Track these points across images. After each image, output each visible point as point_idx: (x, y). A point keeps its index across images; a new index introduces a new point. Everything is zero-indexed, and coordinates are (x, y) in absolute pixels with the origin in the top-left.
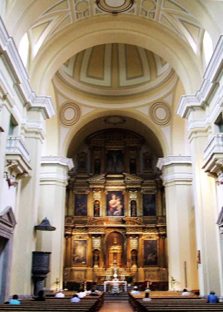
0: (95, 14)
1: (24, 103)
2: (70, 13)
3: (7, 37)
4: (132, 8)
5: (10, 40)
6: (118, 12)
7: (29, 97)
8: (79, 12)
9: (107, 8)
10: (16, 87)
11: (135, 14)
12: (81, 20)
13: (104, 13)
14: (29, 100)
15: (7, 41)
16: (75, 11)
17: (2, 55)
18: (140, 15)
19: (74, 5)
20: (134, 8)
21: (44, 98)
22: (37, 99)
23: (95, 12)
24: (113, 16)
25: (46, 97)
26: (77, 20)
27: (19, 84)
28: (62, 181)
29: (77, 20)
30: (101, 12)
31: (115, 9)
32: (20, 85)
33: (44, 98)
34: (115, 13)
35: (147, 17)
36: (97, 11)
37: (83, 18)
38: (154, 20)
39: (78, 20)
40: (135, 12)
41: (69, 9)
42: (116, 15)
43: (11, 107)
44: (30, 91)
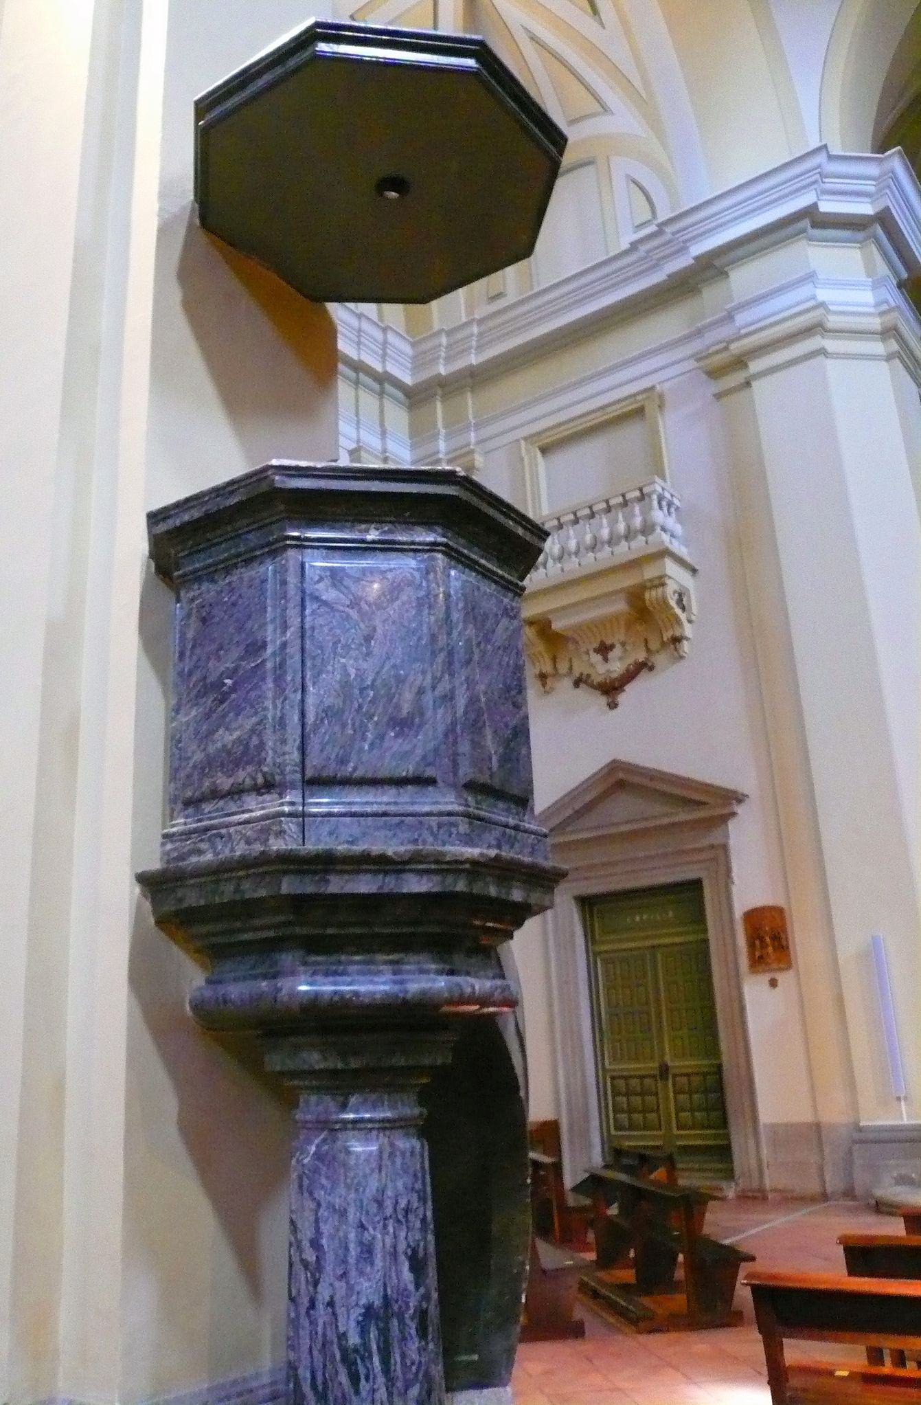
28: (876, 323)
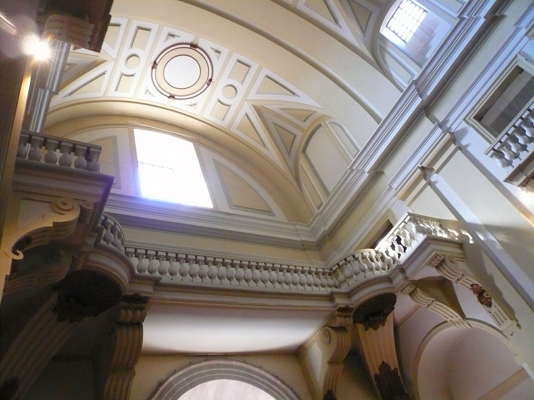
5: (465, 16)
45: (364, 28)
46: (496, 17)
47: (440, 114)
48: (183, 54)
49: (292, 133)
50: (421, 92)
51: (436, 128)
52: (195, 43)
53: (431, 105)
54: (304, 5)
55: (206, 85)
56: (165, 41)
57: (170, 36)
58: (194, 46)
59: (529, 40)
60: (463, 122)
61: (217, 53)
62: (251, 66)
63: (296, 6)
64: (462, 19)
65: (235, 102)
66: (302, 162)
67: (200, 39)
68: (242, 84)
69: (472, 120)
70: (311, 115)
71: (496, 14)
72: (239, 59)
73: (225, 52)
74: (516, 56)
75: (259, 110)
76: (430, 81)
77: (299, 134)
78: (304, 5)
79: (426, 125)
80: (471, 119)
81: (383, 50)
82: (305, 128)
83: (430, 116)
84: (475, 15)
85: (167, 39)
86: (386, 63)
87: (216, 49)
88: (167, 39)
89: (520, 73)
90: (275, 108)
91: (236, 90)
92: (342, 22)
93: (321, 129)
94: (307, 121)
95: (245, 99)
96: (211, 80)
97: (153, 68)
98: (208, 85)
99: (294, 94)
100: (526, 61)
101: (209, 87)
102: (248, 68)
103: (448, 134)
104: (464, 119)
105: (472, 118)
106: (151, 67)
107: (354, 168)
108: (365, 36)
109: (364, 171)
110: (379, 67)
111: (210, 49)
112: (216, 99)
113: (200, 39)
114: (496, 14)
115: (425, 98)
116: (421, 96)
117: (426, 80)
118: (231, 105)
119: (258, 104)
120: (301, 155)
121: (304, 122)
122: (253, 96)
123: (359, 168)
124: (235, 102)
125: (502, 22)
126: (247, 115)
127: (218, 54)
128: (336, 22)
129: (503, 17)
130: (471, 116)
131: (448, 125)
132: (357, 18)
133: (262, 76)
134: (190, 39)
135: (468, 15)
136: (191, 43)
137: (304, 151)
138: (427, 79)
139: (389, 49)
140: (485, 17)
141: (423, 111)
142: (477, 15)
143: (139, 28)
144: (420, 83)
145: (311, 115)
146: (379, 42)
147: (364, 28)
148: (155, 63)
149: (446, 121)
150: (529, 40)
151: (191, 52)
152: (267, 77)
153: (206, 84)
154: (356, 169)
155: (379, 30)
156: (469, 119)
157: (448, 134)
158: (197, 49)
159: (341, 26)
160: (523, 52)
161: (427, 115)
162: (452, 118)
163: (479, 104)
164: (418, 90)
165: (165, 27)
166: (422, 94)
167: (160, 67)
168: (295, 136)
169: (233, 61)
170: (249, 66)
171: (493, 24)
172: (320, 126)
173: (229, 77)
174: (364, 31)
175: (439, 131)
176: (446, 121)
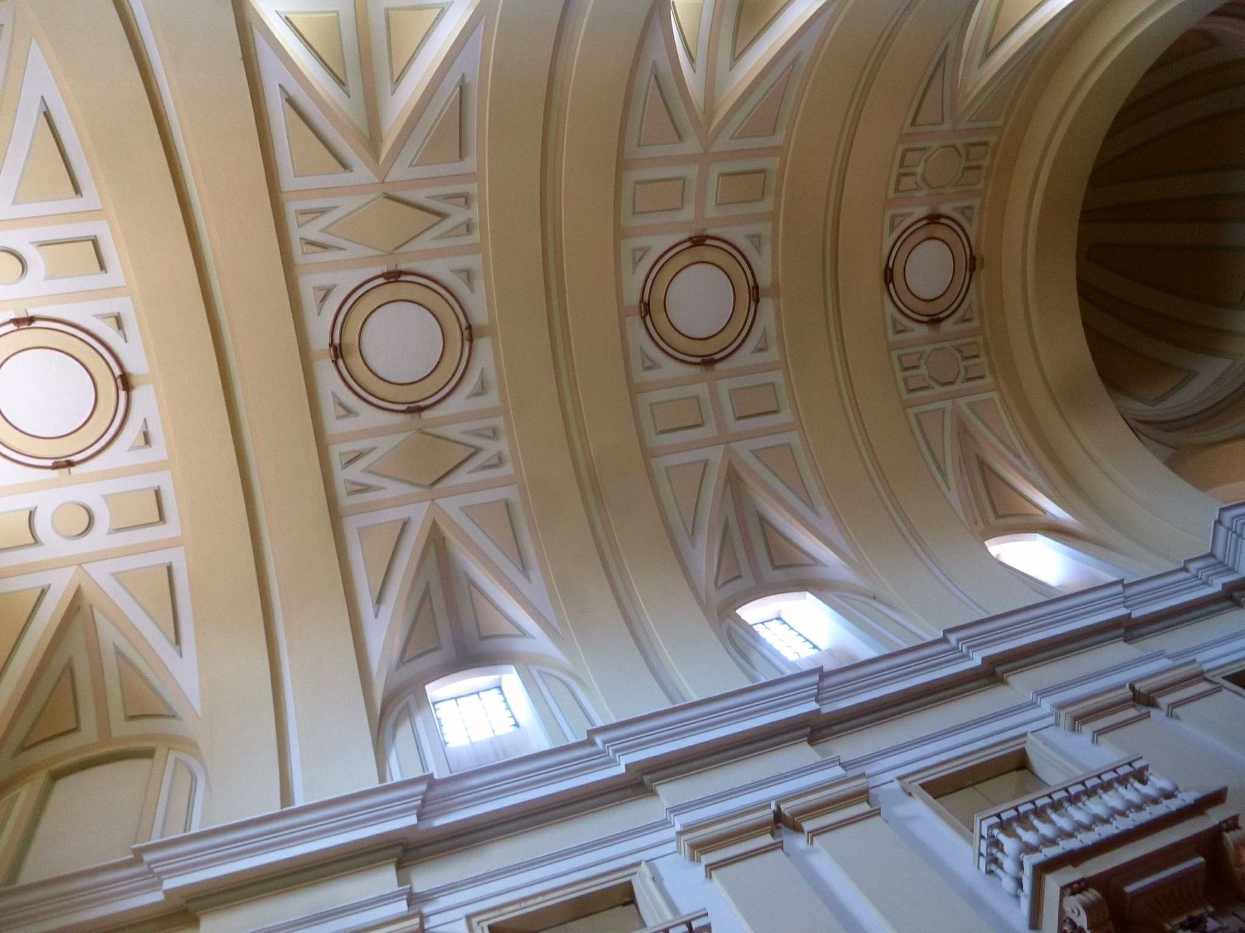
0: (976, 323)
1: (1229, 603)
2: (962, 402)
3: (944, 647)
4: (958, 217)
5: (598, 740)
6: (971, 251)
7: (1206, 583)
8: (963, 373)
9: (952, 295)
10: (1136, 633)
11: (977, 203)
12: (991, 366)
13: (972, 295)
14: (1217, 586)
15: (955, 649)
16: (959, 386)
17: (999, 670)
18: (981, 185)
19: (939, 390)
20: (956, 209)
21: (1222, 530)
22: (1219, 553)
23: (966, 326)
24: (982, 267)
25: (1219, 522)
26: (989, 379)
27: (1132, 616)
29: (989, 379)
30: (970, 307)
31: (962, 261)
32: (1136, 614)
33: (1222, 530)
34: (973, 264)
35: (986, 163)
36: (965, 320)
37: (983, 359)
38: (992, 139)
39: (988, 373)
40: (968, 203)
41: (948, 404)
42: (982, 259)
43: (1199, 677)
44: (1183, 575)
45: (408, 656)
46: (641, 783)
47: (424, 879)
48: (92, 370)
49: (78, 720)
50: (426, 809)
51: (398, 896)
52: (133, 381)
53: (423, 851)
54: (358, 529)
55: (49, 463)
56: (96, 316)
57: (114, 319)
58: (125, 382)
59: (675, 852)
60: (463, 923)
61: (142, 437)
62: (165, 523)
63: (347, 516)
64: (590, 742)
65: (54, 545)
66: (25, 795)
67: (151, 387)
68: (109, 533)
69: (482, 928)
70: (161, 716)
71: (646, 778)
72: (162, 489)
73: (158, 451)
74: (638, 864)
75: (76, 607)
76: (459, 804)
77: (89, 732)
78: (358, 529)
79: (385, 879)
80: (482, 924)
81: (408, 713)
82: (115, 734)
83: (401, 871)
84: (615, 751)
85: (105, 317)
86: (394, 736)
87: (150, 433)
88: (105, 317)
89: (624, 904)
90: (109, 635)
91: (82, 533)
92: (387, 609)
93: (145, 763)
94: (135, 723)
95: (79, 562)
96: (70, 464)
97: (17, 321)
98: (56, 466)
99: (178, 641)
100: (652, 881)
101: (49, 471)
102: (158, 519)
103: (417, 920)
104: (469, 918)
105: (485, 925)
106: (13, 316)
107: (147, 857)
108: (397, 668)
109: (160, 882)
110: (376, 733)
111: (142, 420)
112: (29, 505)
113: (151, 387)
114: (646, 778)
115: (424, 826)
116: (420, 816)
117: (454, 794)
118: (43, 544)
119: (89, 594)
120: (41, 778)
121: (126, 720)
122: (101, 573)
123: (159, 866)
124: (54, 545)
125: (643, 801)
126: (43, 592)
127: (142, 442)
128: (379, 600)
129: (652, 793)
130: (487, 920)
131: (427, 909)
132: (413, 626)
133: (163, 557)
134: (136, 364)
135: (605, 742)
136: (129, 373)
137: (56, 776)
138: (457, 795)
139: (419, 720)
140: (627, 766)
141: (399, 850)
142: (617, 755)
143: (95, 242)
144: (440, 790)
145: (161, 716)
146: (410, 698)
147: (408, 656)
148: (31, 320)
149: (427, 897)
150: (675, 852)
151: (108, 386)
152: (169, 569)
153: (53, 461)
154: (150, 863)
155: (427, 684)
156: (479, 923)
157: (417, 920)
158: (123, 394)
159: (380, 615)
160: (653, 864)
161: (399, 867)
162: (445, 901)
163: (517, 906)
164: (424, 801)
165: (128, 300)
166: (425, 814)
167: (27, 336)
168: (76, 730)
169: (149, 481)
170: (162, 518)
171: (629, 791)
172: (148, 754)
173: (105, 497)
174: (402, 661)
175: (401, 907)
176: (427, 897)
